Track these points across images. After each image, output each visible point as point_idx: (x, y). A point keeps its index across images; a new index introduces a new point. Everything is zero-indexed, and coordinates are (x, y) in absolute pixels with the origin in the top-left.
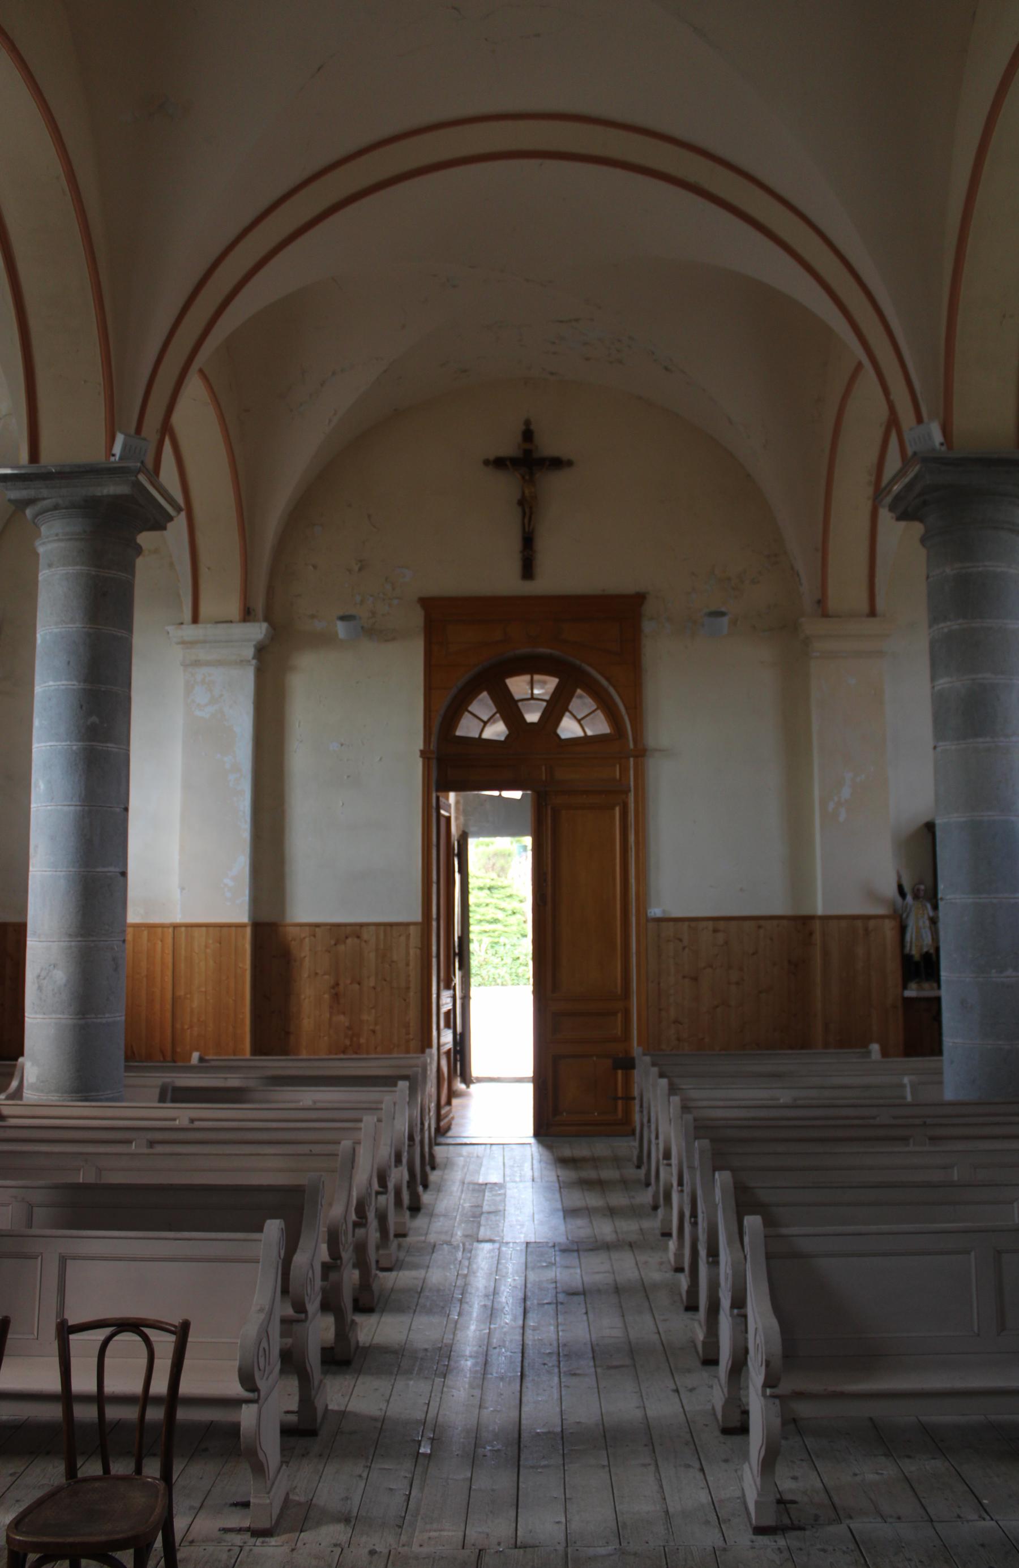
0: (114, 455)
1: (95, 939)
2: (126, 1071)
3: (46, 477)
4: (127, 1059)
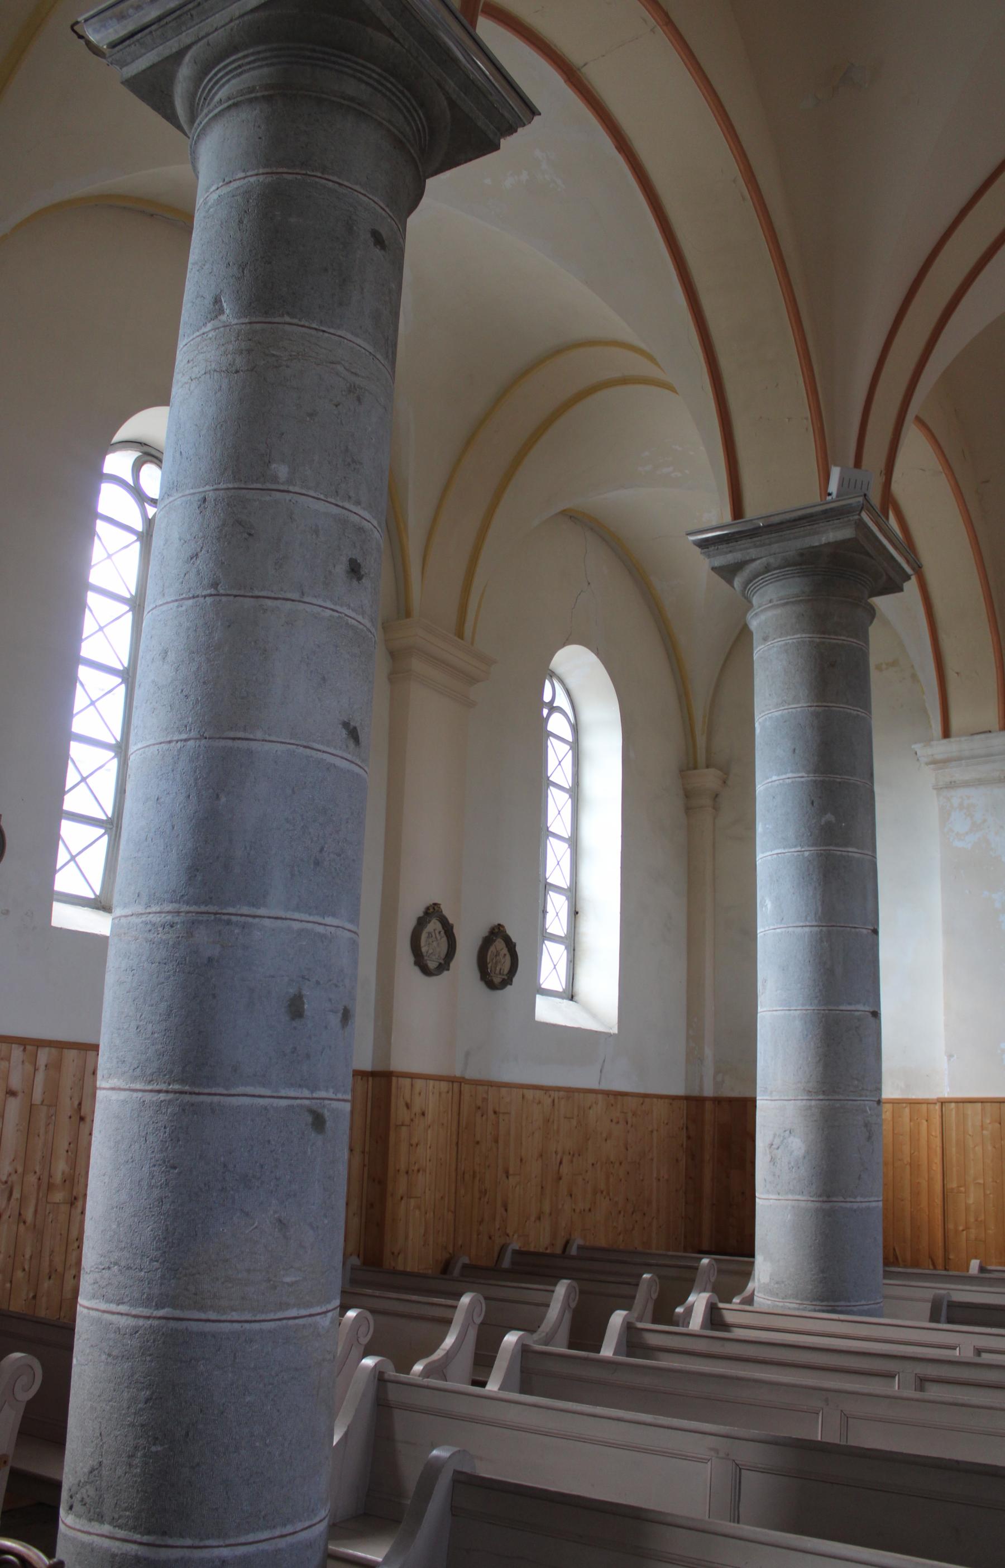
0: (830, 494)
1: (841, 1097)
2: (884, 1278)
3: (753, 533)
4: (886, 1263)
